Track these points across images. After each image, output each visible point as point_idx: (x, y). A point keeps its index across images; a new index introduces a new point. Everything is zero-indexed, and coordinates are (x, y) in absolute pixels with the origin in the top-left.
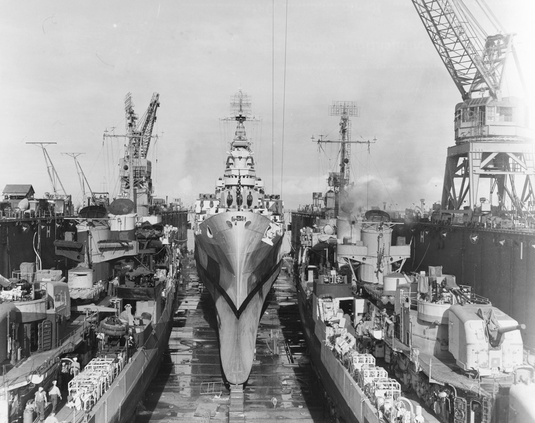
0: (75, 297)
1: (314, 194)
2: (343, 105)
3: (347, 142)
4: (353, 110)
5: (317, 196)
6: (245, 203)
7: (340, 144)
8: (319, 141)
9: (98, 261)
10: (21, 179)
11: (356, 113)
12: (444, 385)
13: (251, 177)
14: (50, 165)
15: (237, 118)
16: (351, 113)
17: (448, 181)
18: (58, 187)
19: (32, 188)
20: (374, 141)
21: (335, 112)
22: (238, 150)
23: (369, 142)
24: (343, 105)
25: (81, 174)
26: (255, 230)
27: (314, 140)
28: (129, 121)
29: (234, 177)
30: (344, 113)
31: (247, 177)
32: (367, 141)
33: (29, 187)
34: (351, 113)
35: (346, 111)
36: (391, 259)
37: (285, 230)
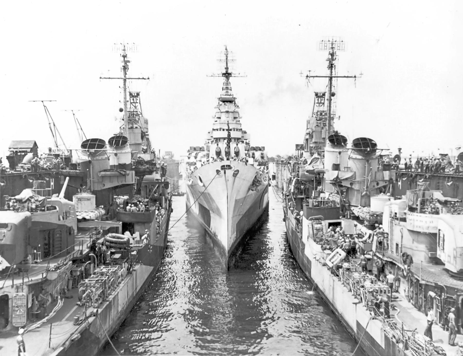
0: (80, 217)
1: (297, 146)
2: (331, 40)
3: (334, 77)
4: (341, 45)
5: (299, 148)
6: (233, 154)
7: (328, 78)
8: (307, 76)
9: (100, 189)
10: (24, 135)
11: (343, 48)
12: (434, 285)
13: (237, 130)
14: (51, 122)
15: (223, 74)
16: (338, 48)
17: (333, 312)
18: (59, 142)
19: (35, 144)
20: (360, 76)
21: (323, 48)
22: (225, 104)
23: (355, 77)
24: (331, 40)
25: (80, 130)
26: (243, 178)
27: (302, 75)
28: (123, 64)
29: (222, 130)
30: (332, 48)
31: (234, 130)
32: (353, 76)
33: (34, 142)
34: (338, 48)
35: (334, 46)
36: (378, 184)
37: (270, 179)
